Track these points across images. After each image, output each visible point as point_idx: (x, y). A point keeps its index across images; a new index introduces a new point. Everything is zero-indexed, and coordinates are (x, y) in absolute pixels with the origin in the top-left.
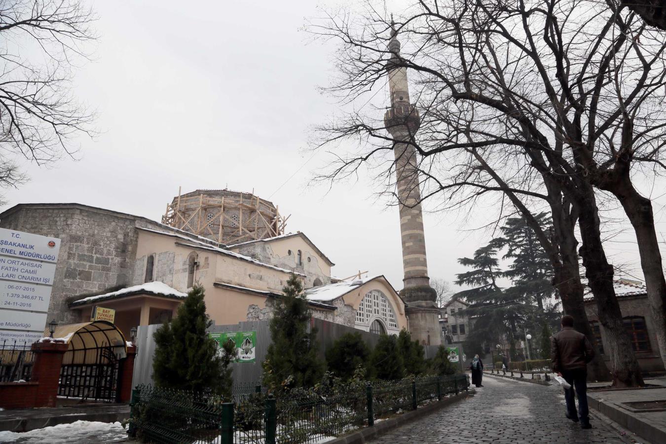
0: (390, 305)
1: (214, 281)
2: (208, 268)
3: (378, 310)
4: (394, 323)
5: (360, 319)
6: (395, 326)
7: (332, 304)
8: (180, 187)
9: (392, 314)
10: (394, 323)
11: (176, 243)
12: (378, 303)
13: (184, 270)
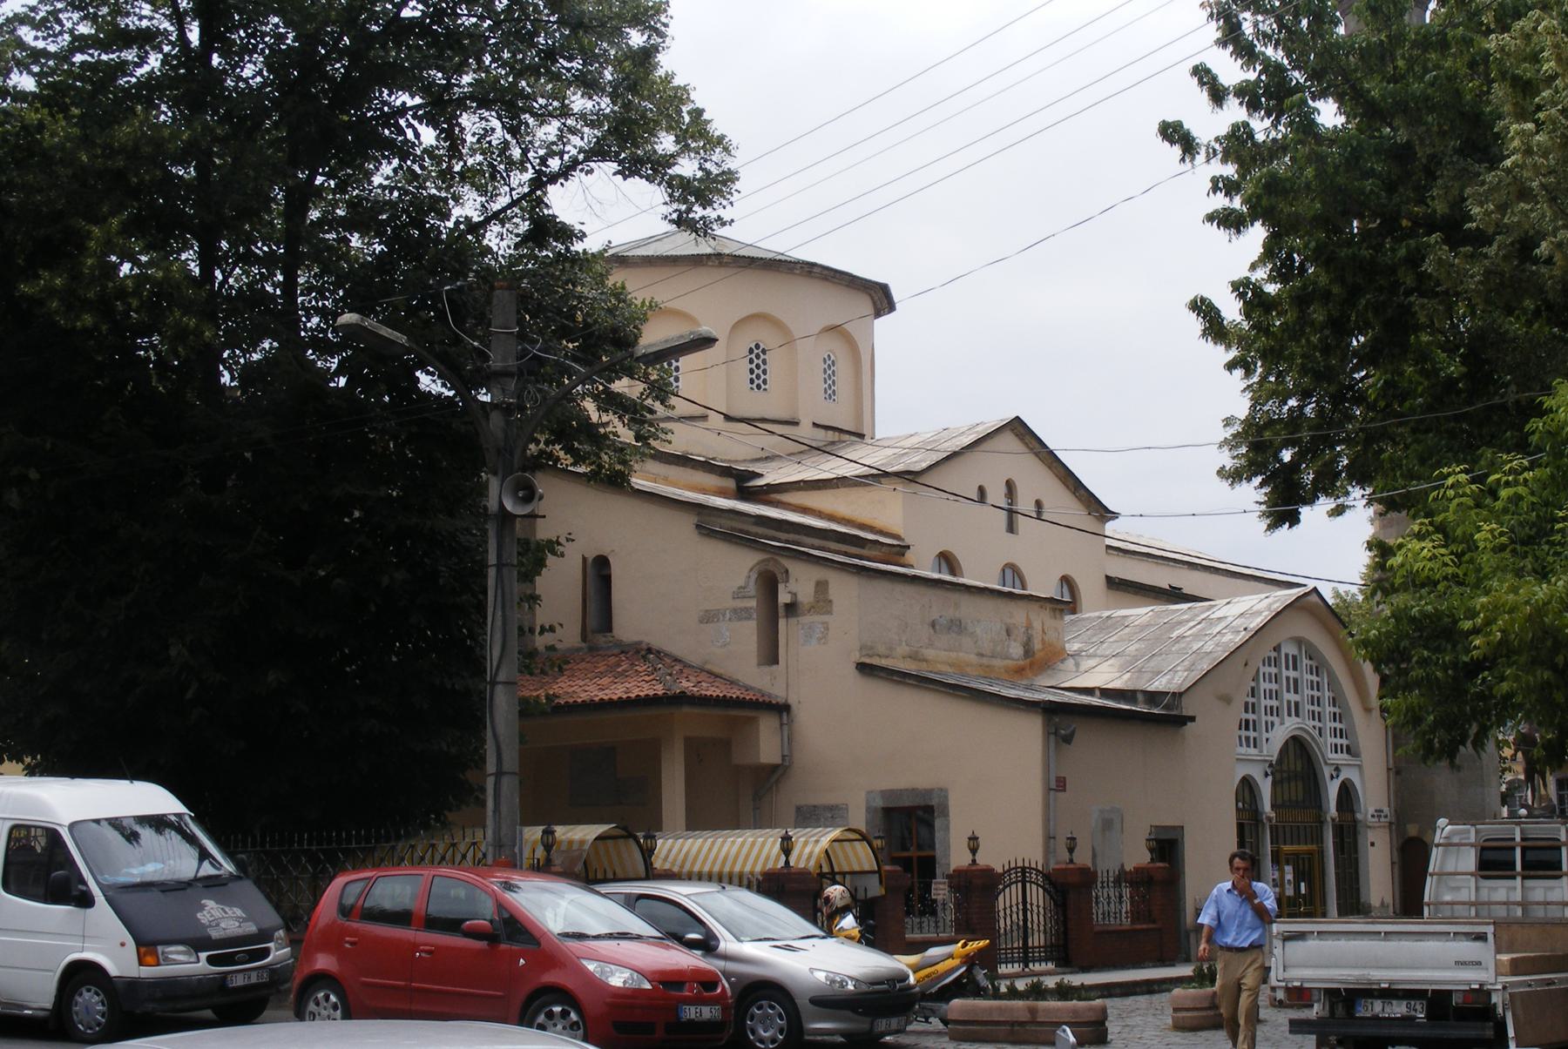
0: (1333, 683)
1: (857, 657)
2: (830, 612)
3: (1297, 704)
4: (1344, 742)
5: (1247, 739)
6: (1349, 751)
7: (1179, 706)
8: (815, 425)
9: (1337, 710)
10: (1344, 742)
11: (698, 526)
12: (1296, 681)
13: (740, 614)
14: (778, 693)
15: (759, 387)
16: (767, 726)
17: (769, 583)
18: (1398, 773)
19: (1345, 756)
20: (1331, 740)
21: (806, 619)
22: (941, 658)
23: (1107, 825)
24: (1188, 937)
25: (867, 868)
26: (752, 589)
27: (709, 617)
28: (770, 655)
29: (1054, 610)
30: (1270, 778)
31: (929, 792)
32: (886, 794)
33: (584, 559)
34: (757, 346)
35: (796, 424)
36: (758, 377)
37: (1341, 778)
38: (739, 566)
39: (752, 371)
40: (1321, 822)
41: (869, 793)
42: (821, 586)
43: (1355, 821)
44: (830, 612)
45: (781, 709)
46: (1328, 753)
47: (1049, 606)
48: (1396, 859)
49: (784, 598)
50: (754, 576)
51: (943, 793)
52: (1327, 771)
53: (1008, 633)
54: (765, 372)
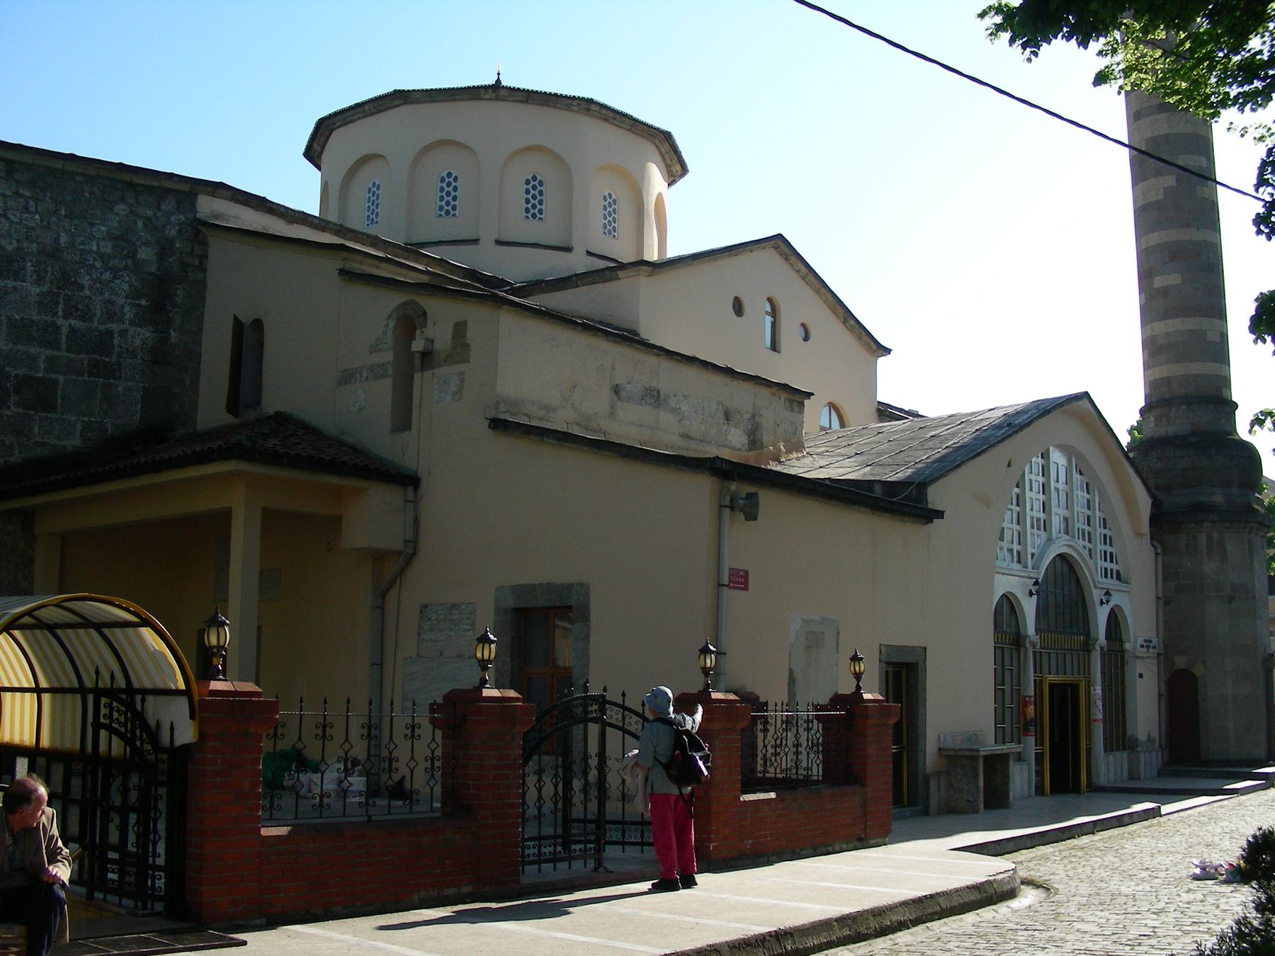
4: (1115, 567)
6: (1119, 577)
8: (589, 253)
14: (409, 462)
15: (534, 216)
17: (409, 322)
18: (1167, 603)
19: (1115, 581)
20: (1101, 564)
21: (441, 371)
22: (629, 426)
24: (927, 782)
25: (26, 685)
27: (346, 378)
28: (403, 421)
29: (791, 401)
30: (1035, 597)
31: (567, 588)
32: (520, 590)
34: (534, 178)
35: (568, 249)
36: (534, 206)
37: (1111, 605)
38: (378, 309)
39: (527, 201)
40: (1087, 647)
41: (498, 589)
42: (460, 329)
43: (1123, 651)
45: (408, 480)
46: (1093, 572)
47: (783, 395)
48: (1163, 692)
50: (392, 324)
51: (583, 590)
52: (1097, 594)
53: (727, 415)
54: (541, 202)
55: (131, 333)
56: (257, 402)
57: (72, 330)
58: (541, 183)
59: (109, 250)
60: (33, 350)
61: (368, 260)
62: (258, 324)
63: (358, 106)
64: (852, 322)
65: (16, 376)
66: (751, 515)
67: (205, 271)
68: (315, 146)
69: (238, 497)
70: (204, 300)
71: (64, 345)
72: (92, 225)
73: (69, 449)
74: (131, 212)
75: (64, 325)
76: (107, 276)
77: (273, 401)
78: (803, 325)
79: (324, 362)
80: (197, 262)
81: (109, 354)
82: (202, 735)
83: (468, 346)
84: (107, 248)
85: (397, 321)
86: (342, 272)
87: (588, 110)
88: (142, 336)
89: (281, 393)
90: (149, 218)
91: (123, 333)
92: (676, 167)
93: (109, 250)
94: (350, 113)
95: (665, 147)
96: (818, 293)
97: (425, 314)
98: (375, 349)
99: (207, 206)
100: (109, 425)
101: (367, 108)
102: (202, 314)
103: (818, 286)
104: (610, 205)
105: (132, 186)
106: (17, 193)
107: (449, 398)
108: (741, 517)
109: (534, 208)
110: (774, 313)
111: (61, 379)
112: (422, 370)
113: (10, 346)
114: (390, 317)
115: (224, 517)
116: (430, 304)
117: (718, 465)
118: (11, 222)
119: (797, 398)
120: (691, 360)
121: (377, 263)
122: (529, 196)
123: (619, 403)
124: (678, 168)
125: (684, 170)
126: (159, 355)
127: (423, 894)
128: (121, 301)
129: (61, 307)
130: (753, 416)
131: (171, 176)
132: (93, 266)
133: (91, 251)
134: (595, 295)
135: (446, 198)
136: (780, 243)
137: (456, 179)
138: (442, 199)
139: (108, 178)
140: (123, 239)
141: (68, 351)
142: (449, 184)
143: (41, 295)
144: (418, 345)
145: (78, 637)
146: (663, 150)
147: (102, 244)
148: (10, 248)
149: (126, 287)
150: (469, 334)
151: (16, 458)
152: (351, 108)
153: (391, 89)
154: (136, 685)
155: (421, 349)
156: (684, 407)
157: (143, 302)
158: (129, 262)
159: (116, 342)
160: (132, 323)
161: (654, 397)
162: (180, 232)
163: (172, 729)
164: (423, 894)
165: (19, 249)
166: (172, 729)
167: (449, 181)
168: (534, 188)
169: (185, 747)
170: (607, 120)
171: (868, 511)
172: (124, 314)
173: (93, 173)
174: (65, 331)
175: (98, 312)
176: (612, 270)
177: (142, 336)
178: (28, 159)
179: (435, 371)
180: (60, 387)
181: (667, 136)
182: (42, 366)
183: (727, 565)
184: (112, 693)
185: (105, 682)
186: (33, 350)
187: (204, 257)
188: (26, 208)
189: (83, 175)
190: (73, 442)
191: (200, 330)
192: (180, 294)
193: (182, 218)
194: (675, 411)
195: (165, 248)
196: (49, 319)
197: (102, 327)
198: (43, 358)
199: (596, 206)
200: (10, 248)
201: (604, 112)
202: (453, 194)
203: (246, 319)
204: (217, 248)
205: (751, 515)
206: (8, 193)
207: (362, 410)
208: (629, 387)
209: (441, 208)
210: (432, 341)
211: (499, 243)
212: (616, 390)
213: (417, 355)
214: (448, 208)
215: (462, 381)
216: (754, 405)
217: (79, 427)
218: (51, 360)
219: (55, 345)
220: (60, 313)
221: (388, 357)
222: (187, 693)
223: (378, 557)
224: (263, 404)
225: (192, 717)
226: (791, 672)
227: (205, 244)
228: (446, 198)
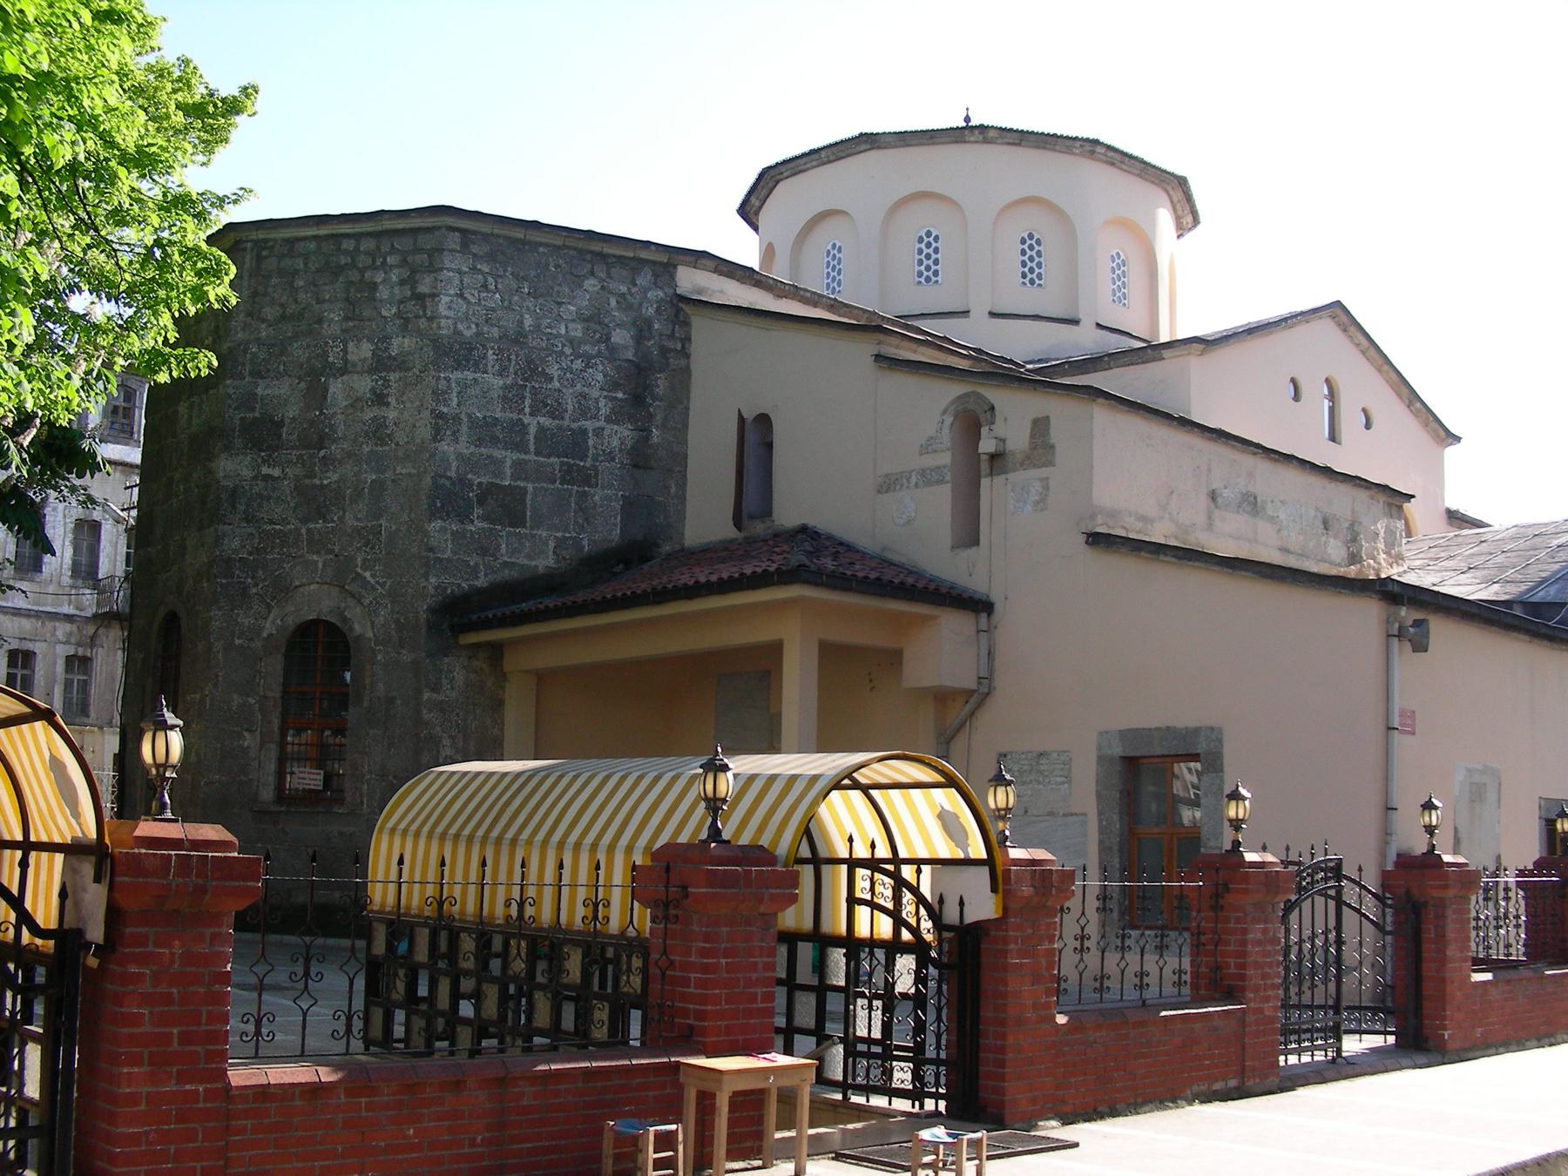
2: (1051, 463)
14: (976, 584)
15: (1032, 282)
16: (953, 625)
17: (971, 421)
22: (1227, 537)
23: (1477, 794)
26: (946, 437)
27: (888, 485)
28: (969, 534)
29: (1390, 505)
32: (1127, 735)
33: (742, 420)
34: (1031, 236)
35: (1075, 322)
36: (1032, 270)
38: (928, 407)
39: (1024, 264)
41: (1101, 733)
42: (1040, 426)
44: (1051, 463)
45: (979, 606)
47: (1382, 498)
49: (987, 446)
50: (949, 420)
53: (1326, 524)
54: (1039, 265)
55: (606, 433)
56: (766, 512)
57: (541, 429)
58: (1039, 242)
59: (579, 334)
60: (498, 453)
61: (906, 344)
62: (764, 421)
63: (812, 152)
64: (1418, 405)
65: (480, 484)
66: (1420, 646)
67: (688, 356)
68: (753, 199)
69: (794, 629)
70: (688, 391)
71: (532, 448)
72: (560, 304)
73: (541, 570)
74: (603, 288)
75: (533, 423)
76: (578, 364)
77: (787, 514)
78: (1364, 411)
79: (859, 462)
80: (679, 347)
81: (583, 458)
82: (1005, 909)
83: (1053, 447)
84: (577, 331)
85: (956, 417)
86: (879, 358)
87: (1093, 152)
88: (620, 435)
89: (798, 501)
90: (623, 295)
91: (598, 432)
92: (1187, 215)
93: (579, 334)
94: (801, 161)
95: (1178, 195)
96: (1379, 371)
97: (993, 408)
98: (925, 450)
99: (689, 280)
100: (585, 542)
101: (823, 154)
102: (687, 408)
103: (1380, 362)
104: (1119, 265)
105: (602, 257)
106: (474, 269)
107: (1029, 508)
108: (1408, 646)
109: (1031, 274)
110: (1332, 396)
111: (530, 487)
112: (991, 474)
113: (472, 449)
114: (944, 412)
115: (774, 650)
116: (1001, 398)
117: (1390, 587)
118: (469, 302)
119: (1396, 501)
120: (1289, 458)
121: (914, 346)
122: (1026, 258)
123: (1217, 513)
124: (1189, 219)
125: (1196, 221)
126: (639, 458)
127: (1195, 1088)
128: (595, 393)
129: (527, 402)
130: (1352, 525)
131: (647, 244)
132: (562, 353)
133: (558, 336)
134: (1113, 375)
135: (926, 262)
136: (1339, 312)
137: (936, 239)
138: (920, 262)
139: (575, 249)
140: (594, 318)
141: (536, 454)
142: (929, 245)
143: (505, 388)
144: (987, 446)
145: (911, 805)
146: (1175, 200)
147: (571, 325)
148: (468, 333)
149: (600, 377)
150: (1052, 432)
151: (481, 582)
152: (804, 155)
153: (856, 133)
154: (823, 853)
155: (992, 450)
156: (1282, 516)
157: (620, 395)
158: (603, 347)
159: (591, 443)
160: (608, 420)
161: (1251, 504)
162: (658, 310)
163: (962, 903)
164: (1195, 1088)
165: (478, 334)
166: (962, 903)
167: (929, 244)
168: (1031, 248)
169: (978, 925)
170: (1113, 164)
171: (1527, 638)
172: (599, 409)
173: (559, 243)
174: (533, 430)
175: (570, 407)
176: (1153, 351)
177: (620, 435)
178: (485, 228)
179: (1011, 476)
180: (529, 497)
181: (1182, 182)
182: (509, 472)
183: (1397, 703)
184: (873, 864)
185: (862, 852)
186: (498, 453)
187: (687, 339)
188: (485, 286)
189: (546, 245)
190: (545, 562)
191: (686, 426)
192: (661, 384)
193: (661, 294)
194: (1273, 520)
195: (642, 331)
196: (515, 416)
197: (574, 426)
198: (509, 463)
199: (1104, 266)
200: (468, 333)
201: (1111, 154)
202: (934, 256)
203: (749, 415)
204: (701, 327)
205: (1420, 646)
206: (465, 269)
207: (915, 526)
208: (1226, 493)
209: (920, 274)
210: (1004, 441)
211: (993, 315)
212: (1213, 496)
213: (984, 457)
214: (929, 273)
215: (1047, 487)
216: (1353, 511)
217: (552, 544)
218: (517, 464)
219: (521, 447)
220: (527, 410)
221: (945, 459)
222: (989, 862)
223: (942, 697)
224: (775, 515)
225: (994, 889)
226: (1456, 830)
227: (686, 324)
228: (926, 262)
